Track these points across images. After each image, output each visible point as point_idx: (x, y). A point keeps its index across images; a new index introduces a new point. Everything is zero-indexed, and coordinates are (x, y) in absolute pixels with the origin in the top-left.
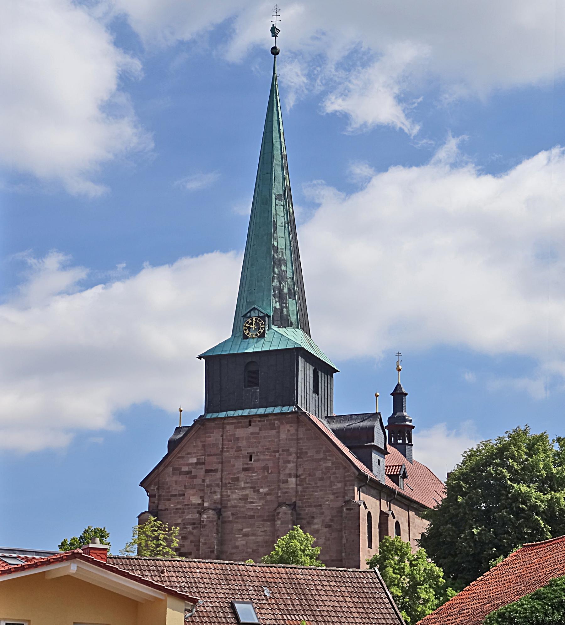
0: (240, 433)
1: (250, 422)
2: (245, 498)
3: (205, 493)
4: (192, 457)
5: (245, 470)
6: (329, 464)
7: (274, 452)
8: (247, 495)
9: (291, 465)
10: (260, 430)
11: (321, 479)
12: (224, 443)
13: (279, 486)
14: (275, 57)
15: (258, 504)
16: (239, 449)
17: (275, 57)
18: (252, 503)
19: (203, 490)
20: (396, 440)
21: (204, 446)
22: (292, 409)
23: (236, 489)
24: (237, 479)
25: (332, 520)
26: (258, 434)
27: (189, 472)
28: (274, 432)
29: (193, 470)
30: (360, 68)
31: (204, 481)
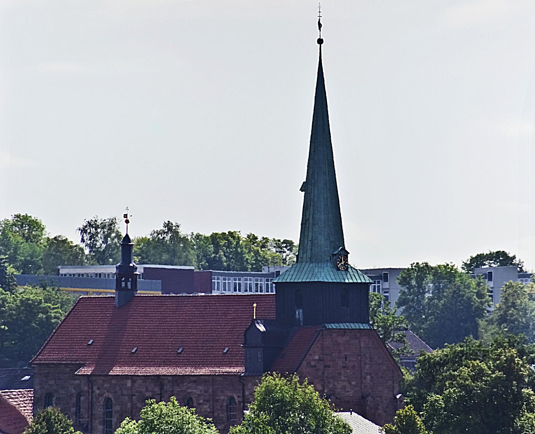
0: (340, 340)
1: (345, 332)
2: (344, 388)
3: (325, 383)
4: (316, 355)
5: (344, 367)
6: (385, 368)
7: (358, 355)
8: (345, 386)
9: (367, 366)
10: (350, 339)
11: (382, 377)
12: (93, 413)
13: (362, 381)
14: (320, 47)
15: (351, 393)
16: (340, 352)
17: (320, 47)
18: (348, 391)
19: (323, 380)
20: (340, 409)
21: (322, 347)
22: (366, 326)
23: (339, 381)
24: (340, 374)
25: (387, 407)
26: (349, 341)
27: (315, 366)
28: (357, 341)
29: (317, 365)
30: (488, 333)
31: (323, 373)
